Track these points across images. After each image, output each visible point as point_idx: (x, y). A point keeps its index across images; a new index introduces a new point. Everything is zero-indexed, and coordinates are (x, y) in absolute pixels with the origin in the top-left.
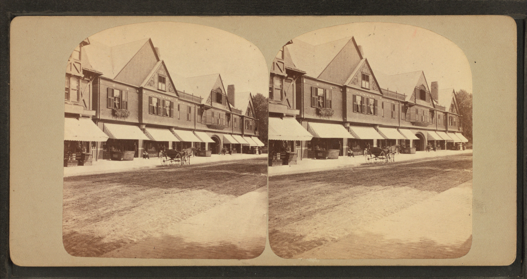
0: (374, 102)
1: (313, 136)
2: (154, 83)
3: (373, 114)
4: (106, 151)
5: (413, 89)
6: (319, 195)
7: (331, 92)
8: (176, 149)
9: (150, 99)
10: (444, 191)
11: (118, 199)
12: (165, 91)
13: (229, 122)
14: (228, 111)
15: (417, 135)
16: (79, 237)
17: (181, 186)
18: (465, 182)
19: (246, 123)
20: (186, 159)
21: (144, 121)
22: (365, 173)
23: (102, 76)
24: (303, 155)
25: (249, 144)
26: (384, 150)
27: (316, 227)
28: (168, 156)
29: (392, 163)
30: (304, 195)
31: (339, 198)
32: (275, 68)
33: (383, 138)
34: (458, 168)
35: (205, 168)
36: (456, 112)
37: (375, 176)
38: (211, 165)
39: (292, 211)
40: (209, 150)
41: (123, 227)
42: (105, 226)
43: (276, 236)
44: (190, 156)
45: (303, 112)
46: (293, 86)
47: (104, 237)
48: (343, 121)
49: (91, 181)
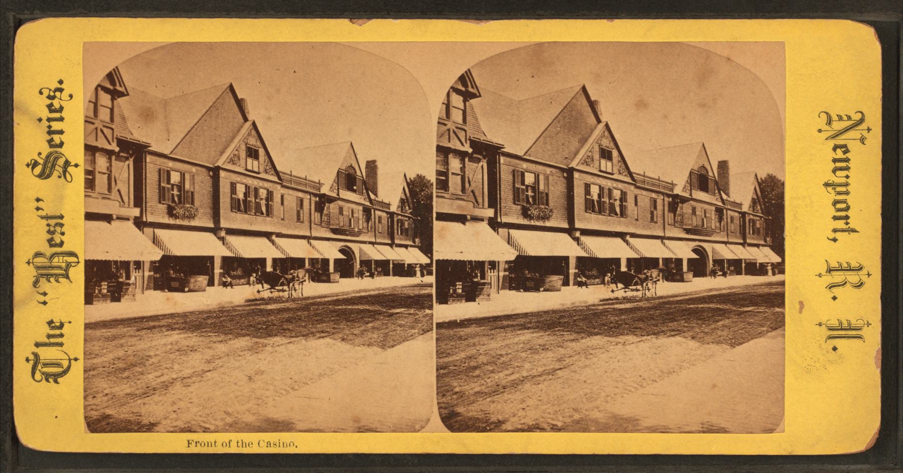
0: (622, 195)
1: (518, 253)
3: (619, 216)
5: (688, 174)
6: (177, 353)
7: (193, 177)
8: (278, 271)
9: (587, 187)
10: (741, 344)
11: (182, 357)
13: (722, 225)
16: (464, 421)
17: (288, 334)
20: (297, 288)
21: (223, 224)
23: (150, 148)
24: (500, 284)
26: (286, 276)
28: (266, 283)
29: (299, 299)
31: (211, 358)
32: (451, 138)
34: (765, 305)
35: (329, 303)
36: (760, 212)
38: (339, 297)
40: (689, 270)
42: (509, 402)
44: (304, 283)
45: (500, 212)
46: (483, 169)
47: (159, 423)
48: (568, 227)
49: (135, 329)
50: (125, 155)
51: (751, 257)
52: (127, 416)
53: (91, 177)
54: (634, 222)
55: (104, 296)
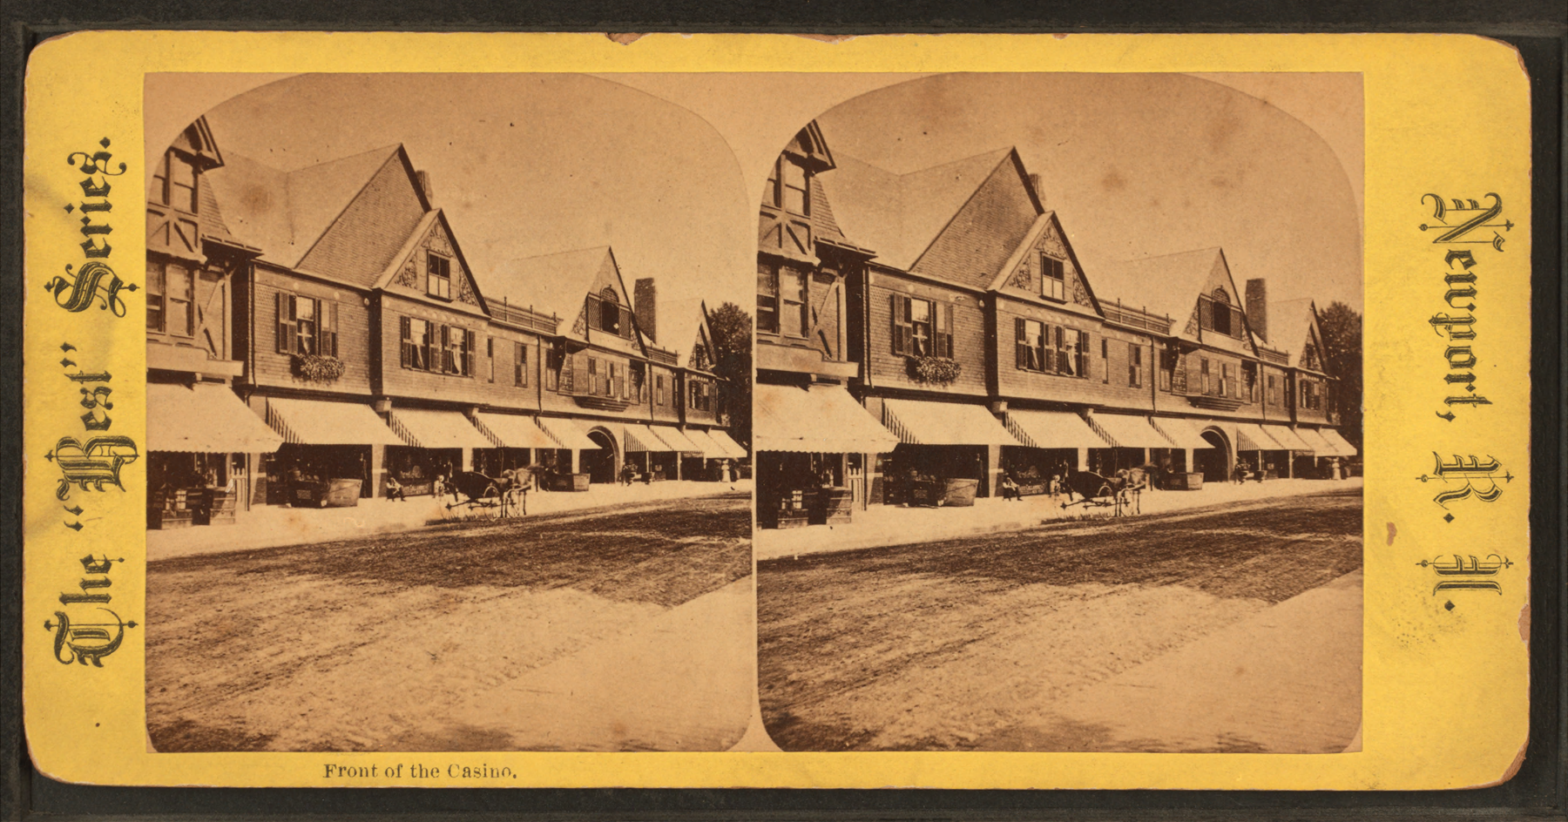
0: (1079, 339)
1: (899, 441)
2: (415, 277)
4: (274, 479)
6: (308, 614)
7: (335, 308)
8: (483, 471)
9: (1020, 324)
10: (1287, 597)
11: (316, 621)
12: (1063, 303)
14: (1250, 354)
15: (1207, 436)
17: (501, 581)
18: (1348, 571)
19: (1301, 391)
21: (388, 389)
22: (1055, 548)
24: (869, 493)
25: (1313, 451)
27: (909, 705)
28: (461, 491)
30: (264, 614)
33: (1105, 445)
34: (1329, 530)
35: (572, 526)
36: (1320, 368)
37: (473, 556)
38: (588, 517)
39: (838, 659)
40: (1197, 469)
41: (330, 703)
43: (792, 733)
44: (528, 492)
46: (224, 291)
49: (234, 571)
50: (217, 269)
51: (1304, 447)
52: (220, 722)
53: (157, 308)
54: (1101, 386)
55: (181, 515)
